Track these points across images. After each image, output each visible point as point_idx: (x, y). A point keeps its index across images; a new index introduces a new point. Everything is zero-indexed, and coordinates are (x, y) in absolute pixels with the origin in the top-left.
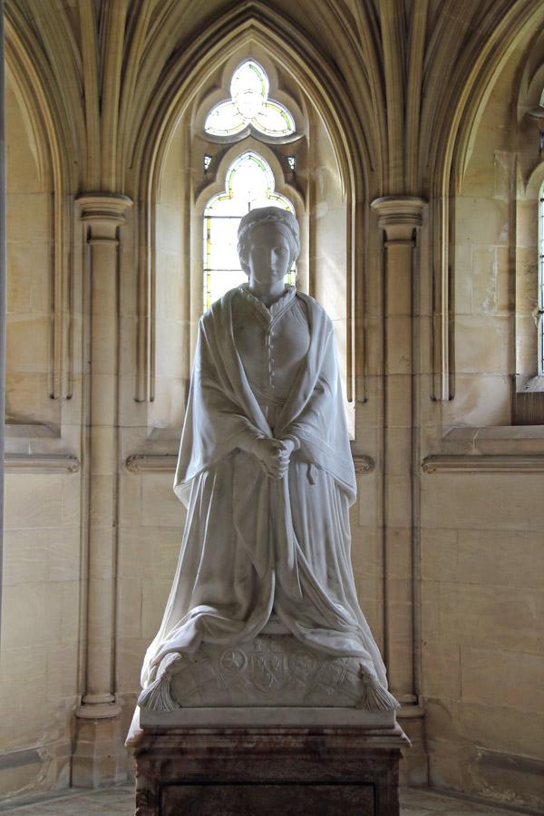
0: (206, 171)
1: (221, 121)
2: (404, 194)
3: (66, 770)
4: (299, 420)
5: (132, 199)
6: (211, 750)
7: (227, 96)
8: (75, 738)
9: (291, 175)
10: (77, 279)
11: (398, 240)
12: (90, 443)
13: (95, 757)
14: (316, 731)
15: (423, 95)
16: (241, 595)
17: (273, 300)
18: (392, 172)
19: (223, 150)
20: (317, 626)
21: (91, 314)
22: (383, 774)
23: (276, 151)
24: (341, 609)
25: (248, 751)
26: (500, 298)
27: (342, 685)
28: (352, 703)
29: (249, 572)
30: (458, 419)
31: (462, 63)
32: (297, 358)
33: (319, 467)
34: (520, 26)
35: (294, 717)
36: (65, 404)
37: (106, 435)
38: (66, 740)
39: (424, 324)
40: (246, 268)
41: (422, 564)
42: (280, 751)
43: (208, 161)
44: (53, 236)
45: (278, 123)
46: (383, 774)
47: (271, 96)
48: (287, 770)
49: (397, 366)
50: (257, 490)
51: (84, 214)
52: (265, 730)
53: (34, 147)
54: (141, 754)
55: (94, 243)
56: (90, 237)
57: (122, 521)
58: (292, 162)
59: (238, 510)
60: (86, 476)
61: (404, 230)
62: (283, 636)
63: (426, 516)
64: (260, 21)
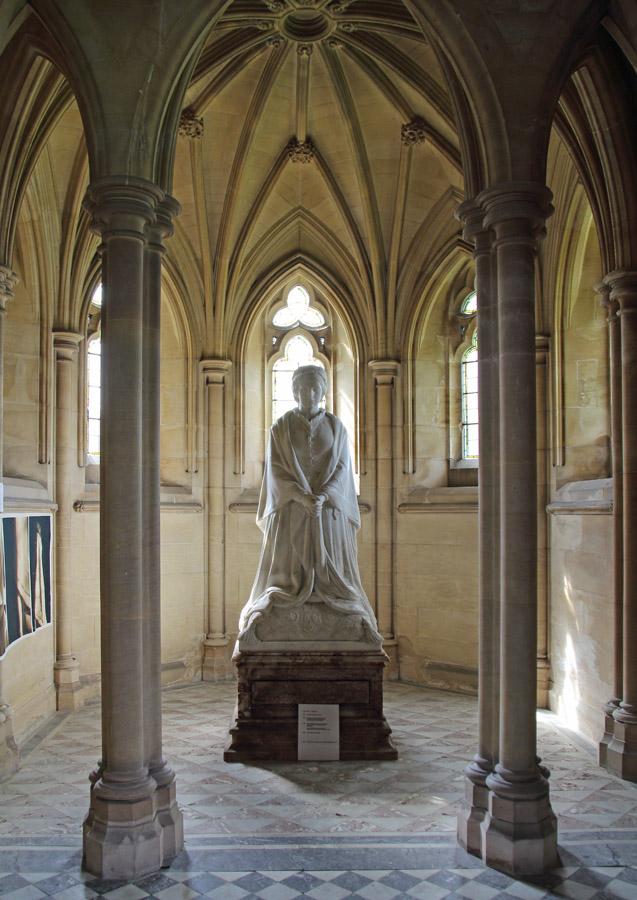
1: (282, 318)
2: (386, 358)
3: (200, 672)
6: (279, 664)
7: (285, 305)
11: (384, 384)
14: (337, 654)
16: (295, 581)
18: (380, 346)
19: (283, 334)
20: (338, 598)
22: (374, 675)
23: (314, 335)
24: (351, 588)
26: (441, 416)
27: (352, 629)
28: (357, 638)
29: (299, 570)
32: (327, 449)
33: (339, 510)
35: (325, 647)
36: (194, 474)
37: (217, 493)
38: (199, 657)
40: (297, 399)
43: (275, 340)
45: (315, 319)
46: (374, 675)
47: (311, 305)
49: (383, 454)
50: (304, 523)
52: (309, 653)
56: (208, 382)
58: (323, 340)
59: (292, 534)
61: (386, 378)
62: (319, 603)
63: (400, 537)
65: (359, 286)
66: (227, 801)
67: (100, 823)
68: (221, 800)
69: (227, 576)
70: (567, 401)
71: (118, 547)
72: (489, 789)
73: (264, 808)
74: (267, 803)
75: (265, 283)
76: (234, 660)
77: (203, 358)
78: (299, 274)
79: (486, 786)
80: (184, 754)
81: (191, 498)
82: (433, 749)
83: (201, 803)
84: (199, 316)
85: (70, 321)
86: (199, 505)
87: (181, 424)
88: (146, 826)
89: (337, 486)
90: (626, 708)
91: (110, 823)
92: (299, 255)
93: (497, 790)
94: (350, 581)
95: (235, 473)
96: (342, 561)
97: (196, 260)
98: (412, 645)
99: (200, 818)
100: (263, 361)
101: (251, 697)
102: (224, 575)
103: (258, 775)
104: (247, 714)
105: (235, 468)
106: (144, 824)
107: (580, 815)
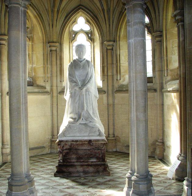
0: (73, 37)
1: (76, 28)
2: (110, 41)
3: (50, 150)
4: (87, 83)
5: (59, 43)
6: (71, 144)
7: (77, 23)
8: (51, 144)
9: (89, 38)
10: (49, 59)
11: (109, 50)
12: (52, 90)
13: (55, 147)
15: (113, 22)
17: (81, 62)
19: (76, 33)
21: (52, 65)
22: (102, 147)
23: (87, 33)
24: (95, 119)
25: (78, 144)
28: (97, 135)
30: (121, 83)
31: (120, 17)
33: (91, 92)
34: (75, 14)
36: (47, 82)
37: (55, 88)
38: (50, 144)
39: (115, 66)
40: (77, 55)
41: (115, 111)
42: (84, 144)
43: (74, 35)
44: (44, 51)
45: (87, 28)
46: (102, 147)
47: (85, 23)
48: (86, 147)
49: (110, 74)
51: (50, 46)
53: (40, 34)
54: (59, 145)
55: (52, 52)
56: (51, 51)
57: (59, 104)
58: (90, 35)
60: (51, 96)
61: (110, 48)
62: (85, 124)
63: (116, 101)
64: (82, 10)
65: (101, 16)
66: (53, 188)
67: (11, 193)
68: (51, 187)
69: (59, 117)
70: (168, 54)
71: (13, 104)
72: (132, 181)
73: (64, 190)
74: (66, 188)
75: (69, 16)
76: (56, 144)
77: (49, 43)
78: (81, 13)
79: (132, 180)
80: (41, 175)
81: (46, 90)
82: (123, 172)
83: (45, 189)
84: (47, 28)
85: (4, 32)
86: (49, 92)
87: (42, 65)
88: (24, 193)
89: (90, 84)
90: (183, 156)
91: (13, 192)
92: (80, 7)
93: (135, 181)
94: (95, 116)
95: (60, 81)
96: (92, 109)
97: (46, 9)
98: (120, 139)
99: (44, 193)
100: (70, 42)
101: (63, 155)
102: (58, 116)
103: (64, 181)
104: (61, 161)
105: (61, 80)
106: (24, 193)
107: (165, 190)
